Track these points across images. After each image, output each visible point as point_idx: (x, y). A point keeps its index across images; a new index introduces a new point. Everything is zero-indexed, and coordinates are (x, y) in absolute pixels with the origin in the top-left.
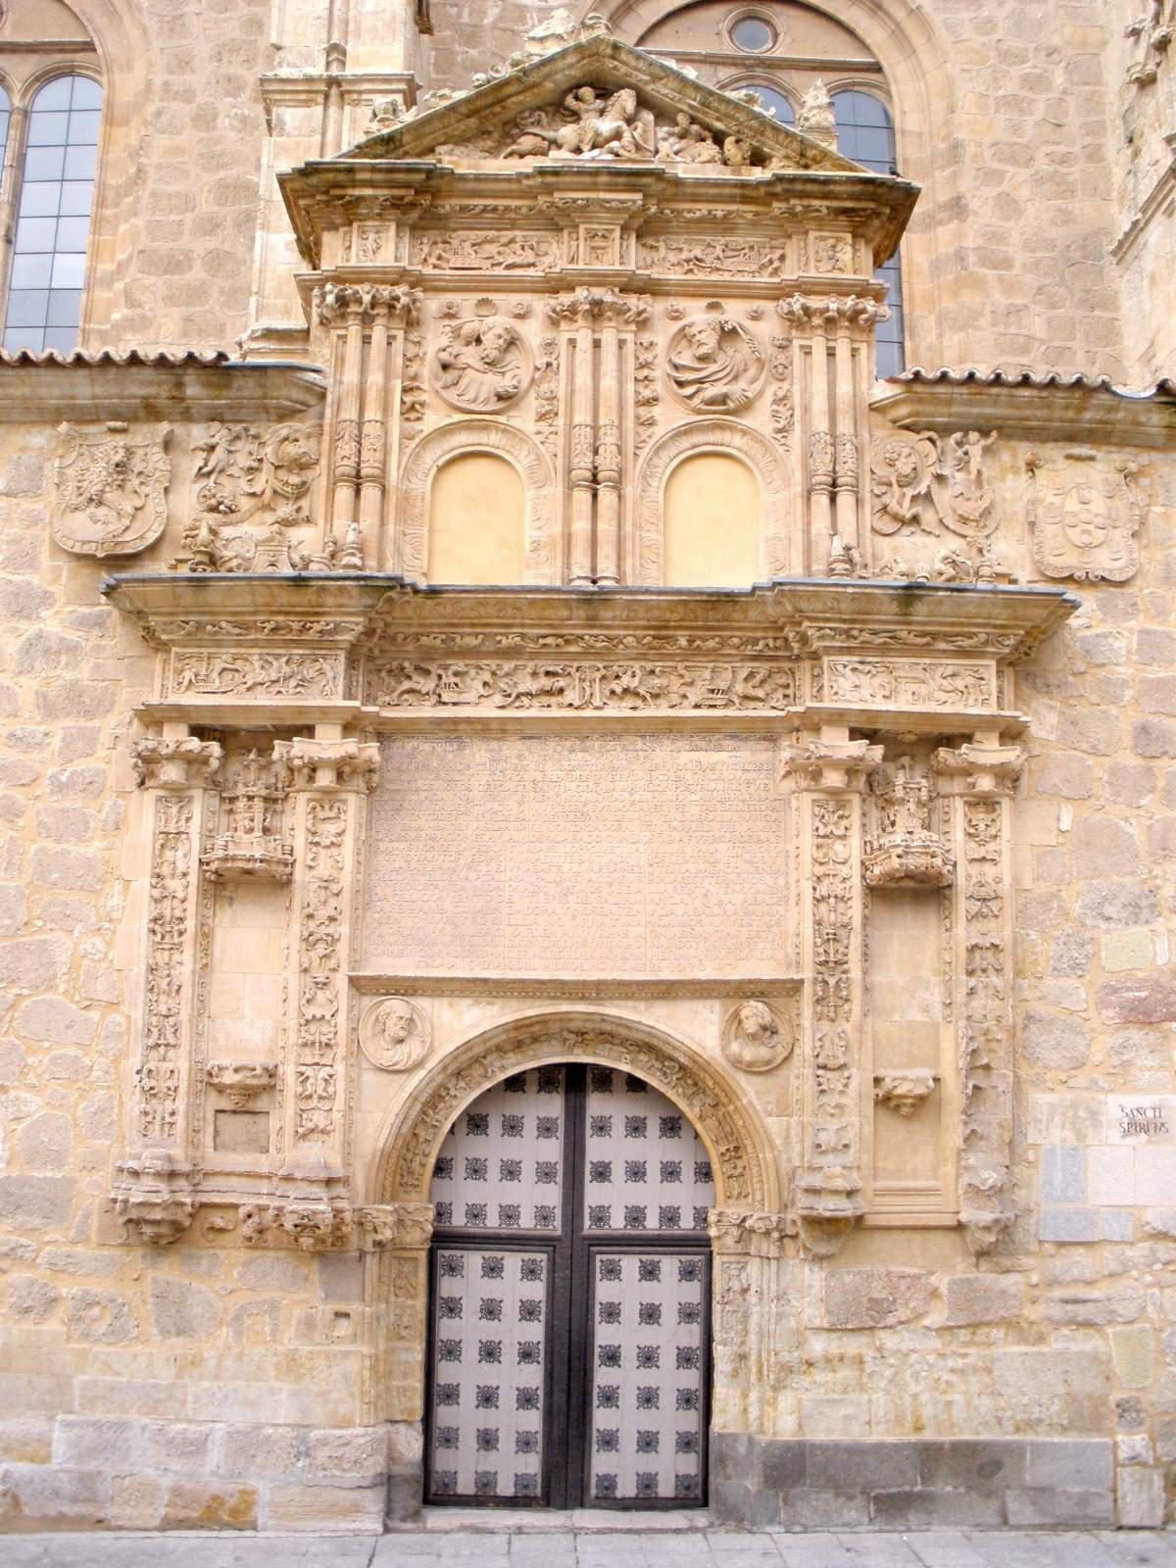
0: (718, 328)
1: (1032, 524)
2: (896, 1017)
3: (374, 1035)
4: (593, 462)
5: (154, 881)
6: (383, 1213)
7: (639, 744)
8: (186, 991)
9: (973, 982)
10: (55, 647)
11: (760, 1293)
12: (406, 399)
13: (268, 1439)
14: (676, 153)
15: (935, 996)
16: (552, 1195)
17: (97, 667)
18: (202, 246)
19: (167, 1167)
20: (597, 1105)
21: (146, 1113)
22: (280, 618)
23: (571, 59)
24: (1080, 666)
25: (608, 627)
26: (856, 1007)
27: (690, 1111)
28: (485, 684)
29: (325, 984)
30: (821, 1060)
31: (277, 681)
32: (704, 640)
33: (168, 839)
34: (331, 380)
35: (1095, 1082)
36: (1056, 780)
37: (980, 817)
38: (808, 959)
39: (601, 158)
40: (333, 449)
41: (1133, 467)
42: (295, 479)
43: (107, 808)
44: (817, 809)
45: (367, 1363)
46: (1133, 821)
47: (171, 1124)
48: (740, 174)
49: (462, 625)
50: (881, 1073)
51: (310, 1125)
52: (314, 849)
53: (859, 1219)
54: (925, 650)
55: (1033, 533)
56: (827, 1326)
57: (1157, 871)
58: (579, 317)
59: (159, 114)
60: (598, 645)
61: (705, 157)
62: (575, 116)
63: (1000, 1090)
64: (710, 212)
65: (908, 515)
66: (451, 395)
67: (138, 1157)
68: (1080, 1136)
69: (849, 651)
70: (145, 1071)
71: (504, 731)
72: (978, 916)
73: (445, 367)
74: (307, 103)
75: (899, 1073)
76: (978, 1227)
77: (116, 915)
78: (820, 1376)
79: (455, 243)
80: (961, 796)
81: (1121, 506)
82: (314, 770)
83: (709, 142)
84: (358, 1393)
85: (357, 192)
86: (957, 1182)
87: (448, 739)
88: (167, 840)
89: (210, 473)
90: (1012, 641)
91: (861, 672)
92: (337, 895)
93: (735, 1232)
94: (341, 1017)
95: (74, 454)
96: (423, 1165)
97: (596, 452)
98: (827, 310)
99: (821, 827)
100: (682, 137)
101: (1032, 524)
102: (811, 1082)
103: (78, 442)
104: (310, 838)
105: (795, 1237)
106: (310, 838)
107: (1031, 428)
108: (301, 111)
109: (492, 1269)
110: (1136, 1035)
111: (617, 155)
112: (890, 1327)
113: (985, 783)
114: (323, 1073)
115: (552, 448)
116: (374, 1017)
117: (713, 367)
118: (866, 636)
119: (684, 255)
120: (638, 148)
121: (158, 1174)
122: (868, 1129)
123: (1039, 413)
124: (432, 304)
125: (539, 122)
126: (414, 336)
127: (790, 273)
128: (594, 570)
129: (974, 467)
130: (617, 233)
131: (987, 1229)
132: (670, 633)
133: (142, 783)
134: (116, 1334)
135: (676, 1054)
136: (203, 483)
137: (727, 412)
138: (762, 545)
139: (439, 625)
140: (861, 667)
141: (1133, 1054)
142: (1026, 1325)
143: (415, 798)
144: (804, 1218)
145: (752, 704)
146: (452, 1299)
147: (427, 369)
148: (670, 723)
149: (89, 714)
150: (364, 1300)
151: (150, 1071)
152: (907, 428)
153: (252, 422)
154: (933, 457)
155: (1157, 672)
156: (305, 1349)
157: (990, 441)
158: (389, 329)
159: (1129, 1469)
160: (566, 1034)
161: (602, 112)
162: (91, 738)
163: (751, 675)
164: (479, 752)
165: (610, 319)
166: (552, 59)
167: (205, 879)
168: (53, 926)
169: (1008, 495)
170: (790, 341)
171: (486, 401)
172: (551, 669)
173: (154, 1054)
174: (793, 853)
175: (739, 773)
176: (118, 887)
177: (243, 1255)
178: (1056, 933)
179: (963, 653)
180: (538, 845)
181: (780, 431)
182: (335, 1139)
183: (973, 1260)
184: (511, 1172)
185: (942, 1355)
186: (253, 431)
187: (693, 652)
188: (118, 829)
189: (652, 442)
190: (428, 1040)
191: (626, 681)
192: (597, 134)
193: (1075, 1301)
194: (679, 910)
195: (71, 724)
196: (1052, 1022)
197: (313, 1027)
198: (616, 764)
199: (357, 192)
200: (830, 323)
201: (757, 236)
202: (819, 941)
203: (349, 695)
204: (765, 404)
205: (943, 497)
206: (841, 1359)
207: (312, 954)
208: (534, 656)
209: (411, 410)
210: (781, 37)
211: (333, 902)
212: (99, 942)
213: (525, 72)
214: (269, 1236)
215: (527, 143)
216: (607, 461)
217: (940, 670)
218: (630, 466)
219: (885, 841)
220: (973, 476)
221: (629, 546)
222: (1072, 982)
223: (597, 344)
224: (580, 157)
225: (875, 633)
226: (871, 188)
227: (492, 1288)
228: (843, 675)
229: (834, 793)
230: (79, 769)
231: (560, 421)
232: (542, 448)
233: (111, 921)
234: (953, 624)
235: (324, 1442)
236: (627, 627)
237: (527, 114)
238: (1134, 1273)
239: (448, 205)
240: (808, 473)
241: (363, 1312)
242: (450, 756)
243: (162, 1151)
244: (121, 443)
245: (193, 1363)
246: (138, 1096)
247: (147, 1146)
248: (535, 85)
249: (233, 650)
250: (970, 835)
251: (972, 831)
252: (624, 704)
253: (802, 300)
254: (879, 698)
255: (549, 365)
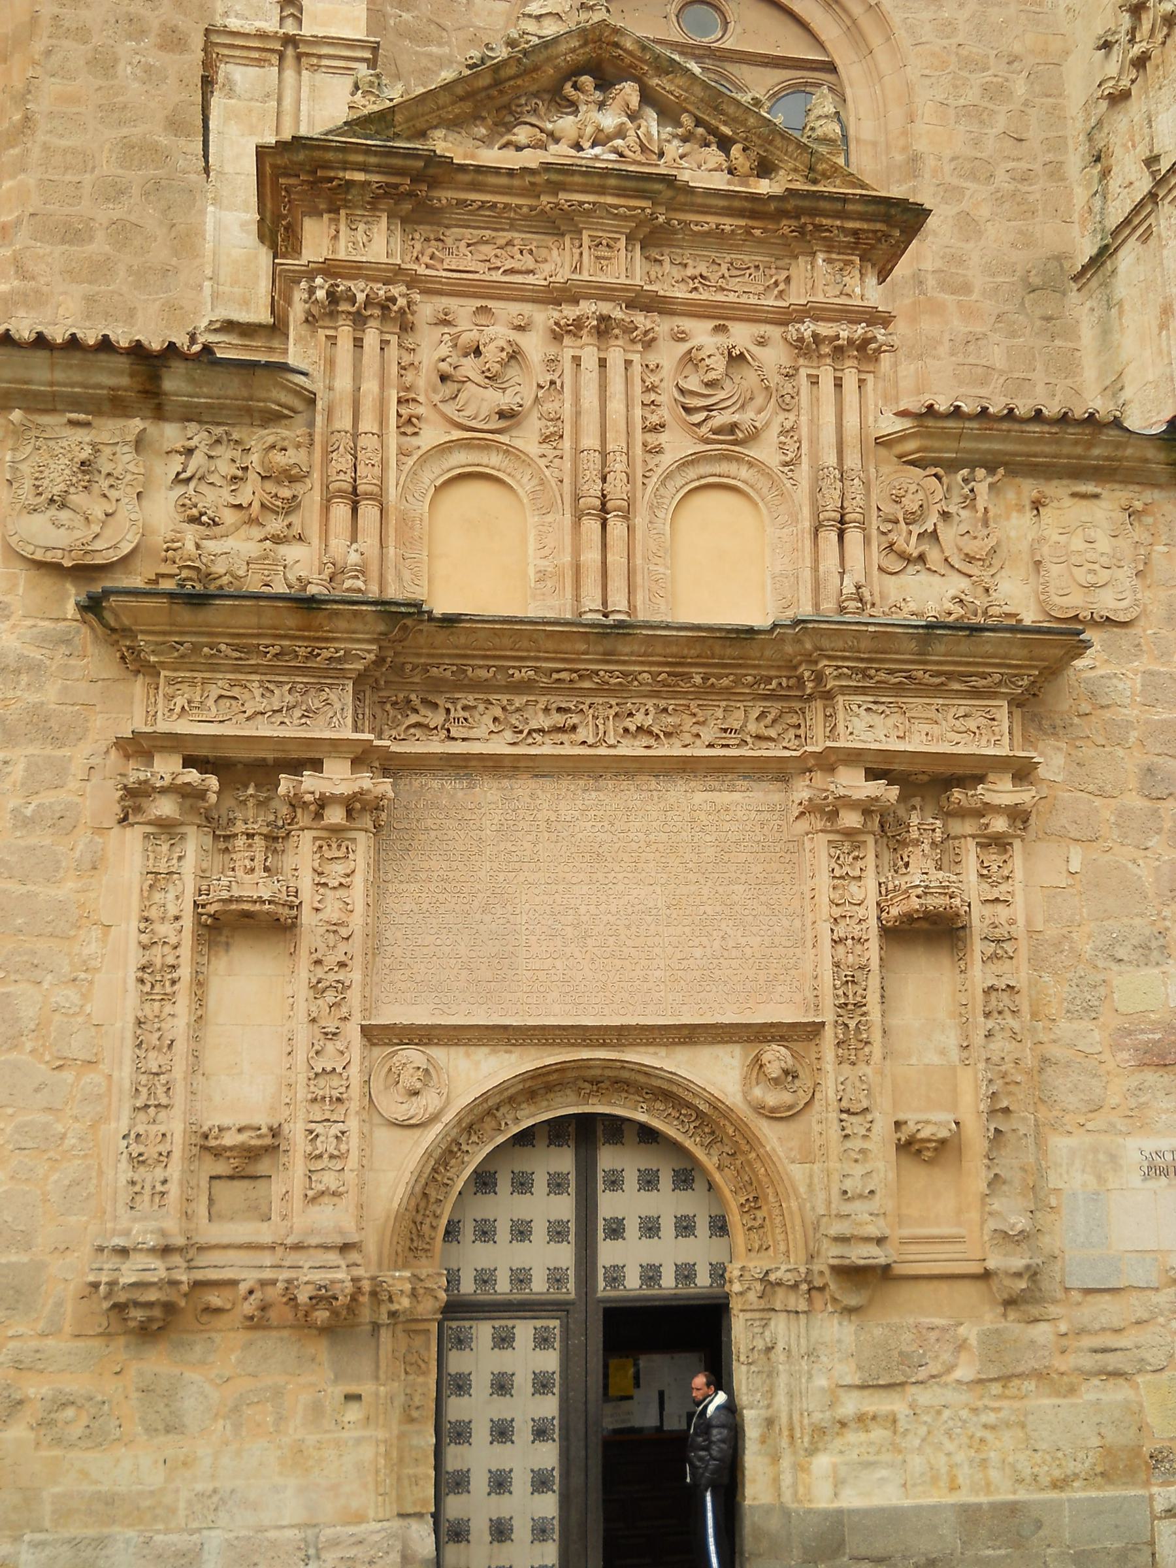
0: (726, 352)
1: (1038, 563)
2: (913, 1061)
3: (387, 1088)
4: (603, 490)
5: (142, 925)
6: (399, 1280)
7: (653, 784)
8: (181, 1047)
9: (990, 1024)
10: (13, 665)
11: (788, 1351)
12: (402, 411)
13: (273, 1543)
14: (681, 157)
15: (951, 1039)
16: (564, 1255)
17: (65, 690)
18: (105, 214)
19: (163, 1242)
20: (608, 1159)
21: (133, 1183)
22: (286, 643)
23: (575, 43)
24: (1085, 707)
25: (624, 663)
26: (877, 1049)
27: (708, 1160)
28: (495, 719)
29: (334, 1034)
30: (844, 1104)
31: (280, 711)
32: (719, 677)
33: (157, 880)
34: (321, 385)
35: (1112, 1125)
36: (1064, 822)
37: (993, 858)
38: (828, 1002)
39: (603, 156)
40: (327, 460)
41: (1138, 505)
42: (286, 493)
43: (80, 847)
44: (832, 851)
45: (382, 1449)
46: (1141, 862)
47: (163, 1194)
48: (748, 186)
49: (474, 657)
50: (901, 1117)
51: (321, 1187)
52: (322, 890)
53: (887, 1267)
54: (938, 690)
55: (1039, 572)
56: (858, 1382)
57: (1167, 912)
58: (584, 332)
59: (48, 53)
60: (613, 681)
61: (711, 165)
62: (572, 106)
63: (1021, 1133)
64: (718, 225)
65: (915, 554)
66: (449, 409)
67: (127, 1233)
68: (1100, 1179)
69: (862, 691)
70: (133, 1135)
71: (516, 768)
72: (995, 957)
73: (444, 378)
74: (259, 63)
75: (923, 1117)
76: (1007, 1273)
77: (93, 964)
78: (853, 1436)
79: (449, 241)
80: (973, 837)
81: (1124, 544)
82: (322, 807)
83: (714, 147)
84: (371, 1486)
85: (348, 175)
86: (982, 1229)
87: (458, 777)
88: (156, 880)
89: (189, 479)
90: (1025, 682)
91: (875, 712)
92: (347, 939)
93: (759, 1287)
94: (354, 1070)
95: (29, 449)
96: (433, 1227)
97: (604, 479)
98: (837, 337)
99: (837, 868)
100: (685, 140)
101: (1038, 563)
102: (836, 1126)
103: (34, 433)
104: (317, 879)
105: (821, 1289)
106: (317, 879)
107: (1036, 465)
108: (253, 71)
109: (503, 1340)
110: (1151, 1077)
111: (621, 155)
112: (922, 1383)
113: (999, 824)
114: (335, 1130)
115: (556, 473)
116: (386, 1069)
117: (722, 395)
118: (882, 676)
119: (690, 272)
120: (644, 148)
121: (153, 1250)
122: (892, 1175)
123: (1047, 449)
124: (427, 309)
125: (535, 111)
126: (409, 341)
127: (797, 297)
128: (605, 603)
129: (981, 504)
130: (622, 243)
131: (1018, 1275)
132: (686, 670)
133: (125, 819)
134: (94, 1437)
135: (696, 1102)
136: (180, 490)
137: (735, 443)
138: (769, 581)
139: (450, 656)
140: (874, 707)
141: (1149, 1096)
142: (1055, 1376)
143: (422, 837)
144: (833, 1268)
145: (765, 745)
146: (459, 1522)
147: (423, 380)
148: (684, 762)
149: (57, 741)
150: (377, 1378)
151: (138, 1135)
152: (912, 463)
153: (233, 425)
154: (939, 494)
155: (1161, 714)
156: (311, 1439)
157: (996, 478)
158: (382, 332)
159: (1166, 1522)
160: (581, 1084)
161: (601, 105)
162: (61, 770)
163: (763, 715)
164: (489, 791)
165: (617, 337)
166: (556, 40)
167: (199, 923)
168: (18, 977)
169: (1013, 534)
170: (797, 370)
171: (487, 419)
172: (563, 705)
173: (142, 1116)
174: (808, 895)
175: (753, 814)
176: (96, 932)
177: (243, 1336)
178: (1069, 975)
179: (976, 693)
180: (554, 887)
181: (786, 464)
182: (348, 1202)
183: (1001, 1309)
184: (521, 1232)
185: (975, 1410)
186: (235, 436)
187: (707, 691)
188: (95, 868)
189: (660, 471)
190: (445, 1091)
191: (639, 718)
192: (599, 130)
193: (1104, 1351)
194: (698, 952)
195: (36, 752)
196: (1068, 1065)
197: (322, 1082)
198: (630, 804)
199: (348, 175)
200: (839, 352)
201: (762, 254)
202: (838, 983)
203: (356, 729)
204: (772, 436)
205: (947, 534)
206: (874, 1418)
207: (320, 1002)
208: (546, 691)
209: (408, 424)
210: (731, 26)
211: (343, 947)
212: (72, 994)
213: (525, 53)
214: (272, 1314)
215: (522, 134)
216: (617, 489)
217: (954, 710)
218: (639, 494)
219: (901, 881)
220: (980, 514)
221: (639, 579)
222: (1086, 1024)
223: (602, 363)
224: (581, 154)
225: (891, 672)
226: (882, 208)
227: (504, 1360)
228: (858, 715)
229: (849, 833)
230: (46, 801)
231: (567, 444)
232: (547, 472)
233: (86, 971)
234: (968, 664)
235: (335, 1543)
236: (642, 663)
237: (523, 101)
238: (1161, 1320)
239: (445, 196)
240: (816, 511)
241: (377, 1395)
242: (460, 794)
243: (153, 1225)
244: (87, 439)
245: (185, 1464)
246: (124, 1164)
247: (135, 1220)
248: (536, 68)
249: (229, 676)
250: (982, 875)
251: (985, 872)
252: (637, 743)
253: (813, 327)
254: (893, 738)
255: (552, 383)
